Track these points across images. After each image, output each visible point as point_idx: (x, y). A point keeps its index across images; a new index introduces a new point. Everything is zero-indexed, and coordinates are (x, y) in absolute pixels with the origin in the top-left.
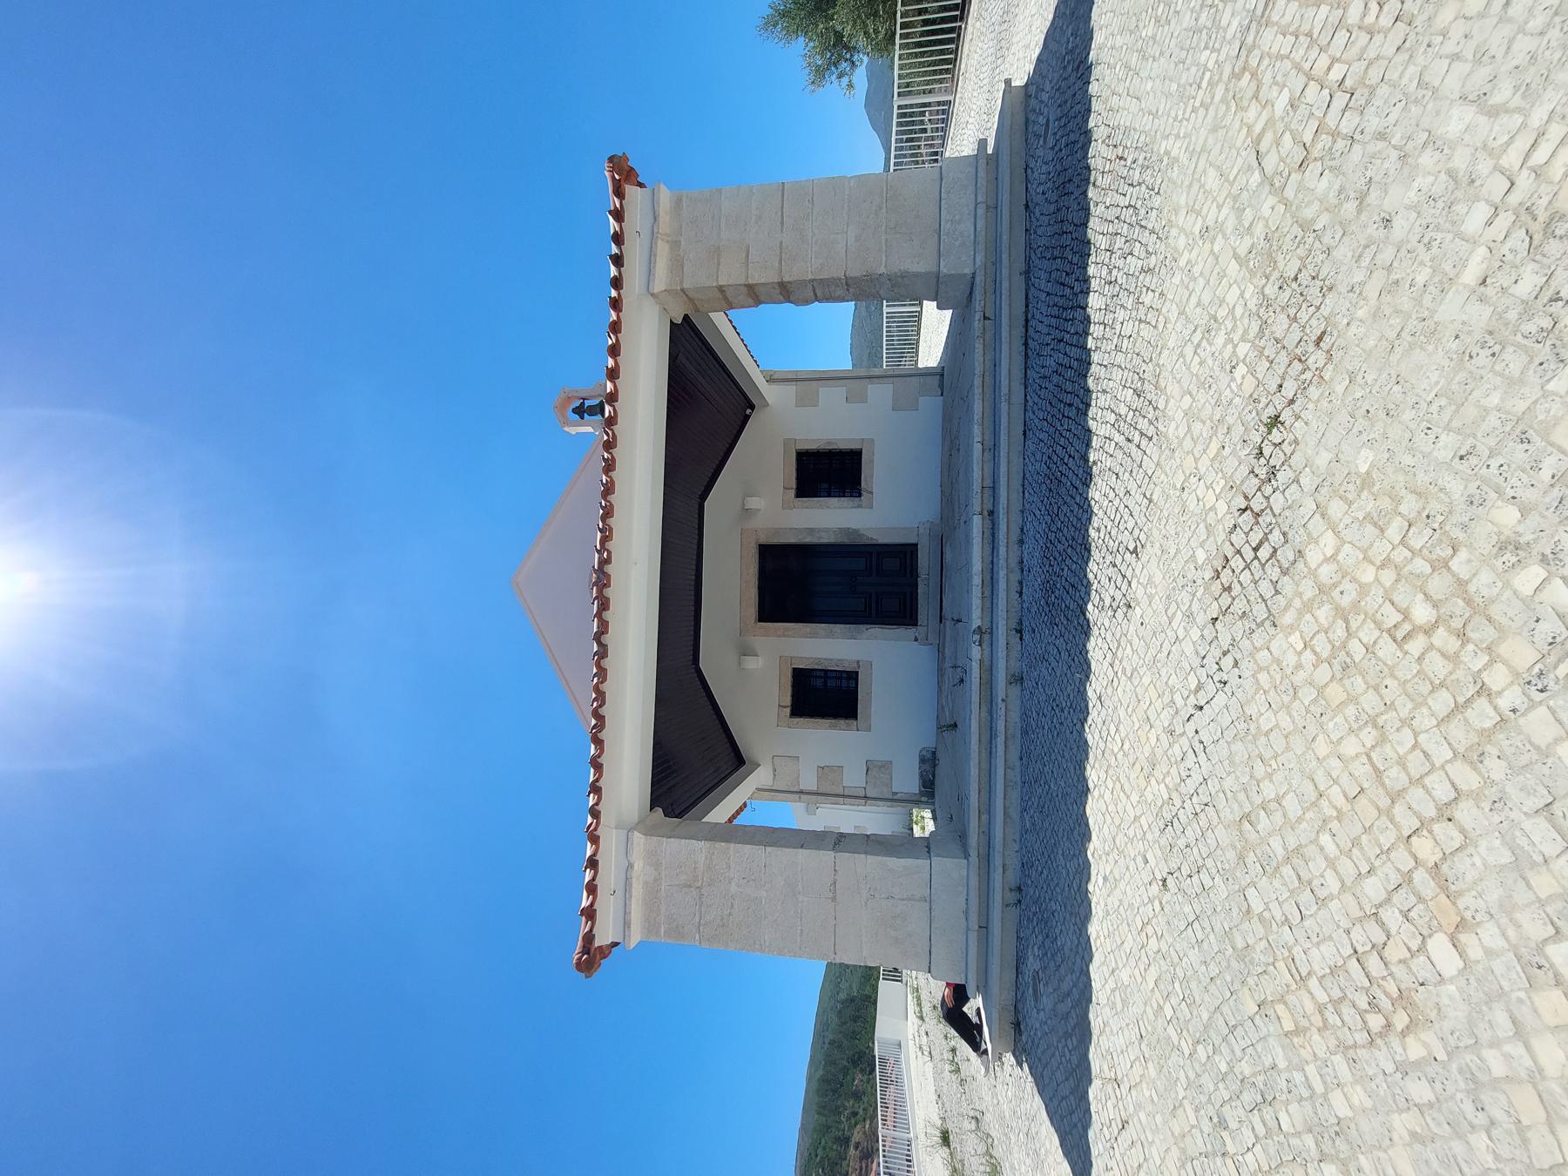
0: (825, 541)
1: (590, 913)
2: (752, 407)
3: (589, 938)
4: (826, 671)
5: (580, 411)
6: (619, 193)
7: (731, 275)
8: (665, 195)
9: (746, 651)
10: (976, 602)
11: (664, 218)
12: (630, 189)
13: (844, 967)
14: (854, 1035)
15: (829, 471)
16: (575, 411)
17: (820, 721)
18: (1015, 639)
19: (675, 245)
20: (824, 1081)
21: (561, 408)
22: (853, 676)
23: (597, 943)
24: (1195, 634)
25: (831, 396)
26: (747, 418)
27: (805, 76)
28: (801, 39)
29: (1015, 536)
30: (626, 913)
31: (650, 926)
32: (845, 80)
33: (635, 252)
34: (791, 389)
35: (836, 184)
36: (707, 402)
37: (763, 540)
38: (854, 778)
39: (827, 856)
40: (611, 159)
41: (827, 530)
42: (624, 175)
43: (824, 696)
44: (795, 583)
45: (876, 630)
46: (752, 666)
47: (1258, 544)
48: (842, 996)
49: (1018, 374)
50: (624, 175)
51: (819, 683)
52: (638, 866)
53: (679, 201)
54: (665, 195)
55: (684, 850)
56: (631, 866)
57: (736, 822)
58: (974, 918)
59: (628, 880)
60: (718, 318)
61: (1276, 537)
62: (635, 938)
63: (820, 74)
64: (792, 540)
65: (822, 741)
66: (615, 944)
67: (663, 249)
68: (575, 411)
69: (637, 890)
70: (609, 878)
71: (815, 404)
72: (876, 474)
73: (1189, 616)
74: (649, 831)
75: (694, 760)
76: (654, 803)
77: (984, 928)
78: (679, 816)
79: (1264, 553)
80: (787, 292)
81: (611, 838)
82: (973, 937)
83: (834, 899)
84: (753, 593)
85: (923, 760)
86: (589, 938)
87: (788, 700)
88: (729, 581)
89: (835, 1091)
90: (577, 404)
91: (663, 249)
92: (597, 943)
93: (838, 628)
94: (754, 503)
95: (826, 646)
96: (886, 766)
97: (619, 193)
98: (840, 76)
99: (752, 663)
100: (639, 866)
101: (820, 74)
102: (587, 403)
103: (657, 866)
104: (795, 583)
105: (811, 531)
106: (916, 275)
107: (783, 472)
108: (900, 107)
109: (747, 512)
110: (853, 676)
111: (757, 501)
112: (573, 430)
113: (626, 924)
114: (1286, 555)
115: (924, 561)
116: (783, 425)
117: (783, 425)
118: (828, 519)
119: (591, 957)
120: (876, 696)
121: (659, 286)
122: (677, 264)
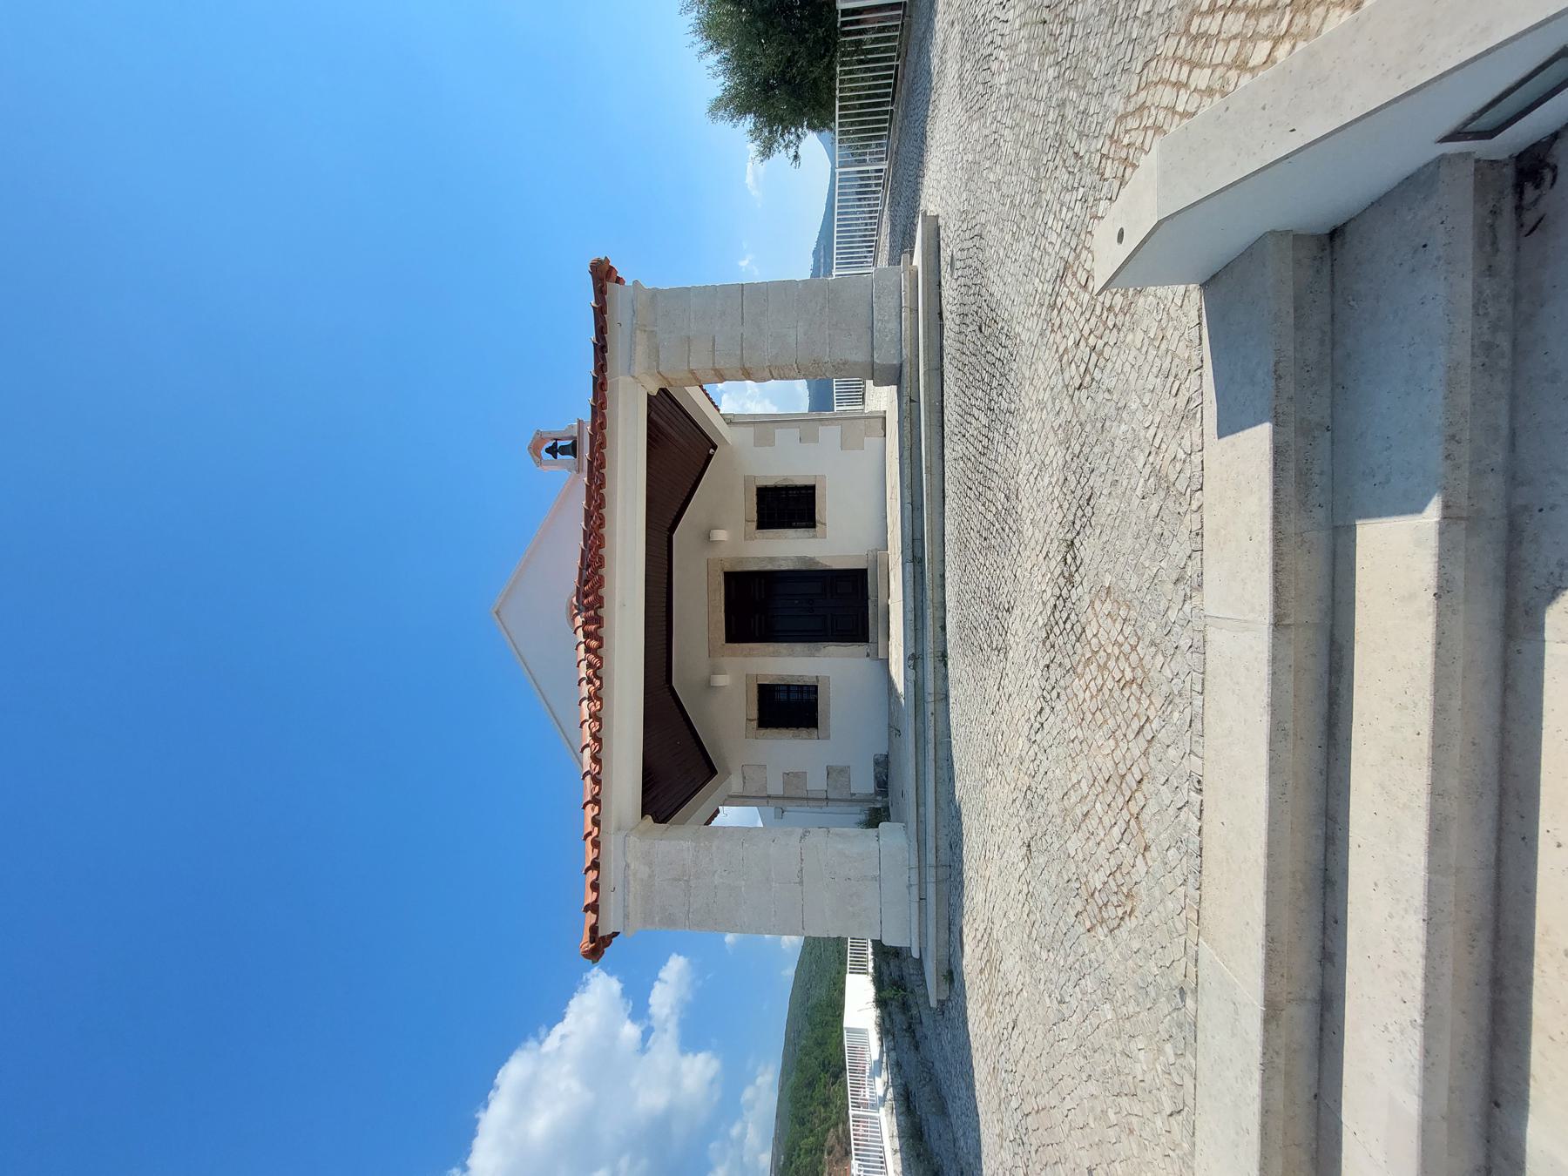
3: (594, 929)
13: (816, 692)
14: (820, 1044)
15: (788, 506)
16: (548, 450)
17: (784, 731)
22: (813, 689)
23: (600, 934)
24: (1039, 673)
26: (710, 457)
27: (753, 148)
34: (749, 431)
37: (728, 568)
41: (786, 559)
43: (788, 708)
48: (813, 1001)
51: (783, 696)
57: (713, 823)
58: (915, 890)
60: (694, 391)
61: (1073, 617)
65: (787, 751)
66: (616, 934)
68: (548, 450)
71: (772, 444)
72: (827, 507)
73: (1036, 661)
75: (678, 770)
76: (645, 811)
78: (664, 821)
79: (1068, 626)
81: (612, 843)
83: (801, 883)
85: (877, 763)
87: (754, 714)
90: (550, 444)
92: (600, 934)
93: (799, 647)
95: (788, 663)
96: (844, 771)
98: (787, 147)
102: (560, 444)
105: (772, 559)
106: (856, 363)
108: (841, 99)
110: (813, 689)
113: (626, 916)
114: (1078, 629)
118: (786, 549)
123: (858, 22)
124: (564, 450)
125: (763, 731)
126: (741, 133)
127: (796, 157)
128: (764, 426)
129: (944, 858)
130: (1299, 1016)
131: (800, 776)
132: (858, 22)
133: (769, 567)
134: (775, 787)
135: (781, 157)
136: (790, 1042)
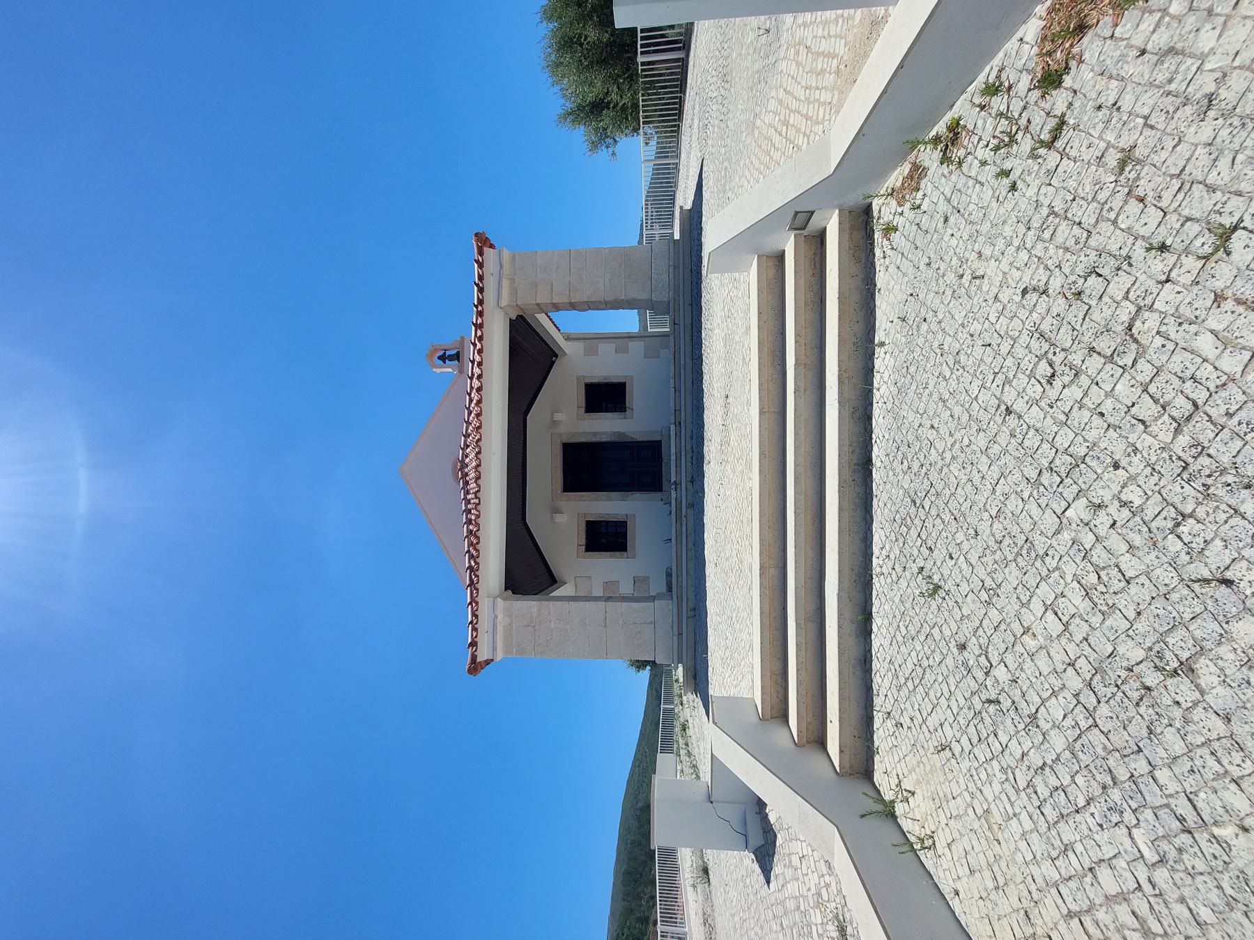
0: (604, 440)
1: (473, 644)
2: (556, 356)
3: (474, 658)
4: (607, 522)
5: (443, 358)
6: (481, 253)
7: (543, 298)
8: (506, 254)
9: (556, 511)
10: (673, 469)
11: (506, 271)
12: (486, 250)
15: (606, 396)
16: (439, 358)
18: (690, 486)
19: (512, 281)
20: (628, 873)
21: (430, 356)
22: (623, 525)
25: (606, 348)
27: (585, 147)
28: (582, 127)
29: (689, 435)
30: (494, 642)
31: (508, 650)
32: (610, 150)
33: (490, 284)
34: (581, 344)
35: (598, 251)
36: (531, 356)
37: (565, 440)
38: (626, 588)
39: (601, 604)
40: (476, 235)
41: (605, 433)
42: (483, 242)
43: (605, 538)
44: (586, 467)
45: (638, 495)
46: (561, 521)
47: (725, 443)
48: (640, 805)
49: (689, 354)
50: (483, 242)
51: (603, 530)
52: (500, 617)
53: (514, 257)
54: (506, 254)
55: (528, 606)
56: (496, 617)
58: (675, 628)
59: (495, 625)
60: (542, 318)
62: (499, 657)
63: (594, 146)
64: (583, 440)
65: (606, 566)
67: (505, 283)
68: (439, 358)
69: (500, 629)
70: (484, 624)
72: (636, 397)
74: (505, 599)
75: (529, 573)
77: (680, 634)
80: (573, 306)
82: (675, 638)
84: (559, 474)
86: (474, 658)
87: (583, 541)
88: (545, 467)
89: (636, 881)
91: (505, 283)
93: (613, 494)
94: (558, 416)
95: (606, 506)
96: (645, 580)
97: (481, 253)
99: (560, 518)
100: (500, 614)
101: (594, 146)
103: (510, 616)
104: (586, 467)
107: (576, 397)
109: (554, 423)
111: (562, 416)
112: (438, 371)
113: (494, 649)
115: (671, 450)
116: (577, 366)
117: (577, 366)
118: (605, 426)
119: (475, 667)
120: (639, 536)
121: (504, 303)
122: (514, 291)
123: (652, 69)
124: (451, 358)
125: (560, 447)
126: (579, 135)
127: (614, 154)
128: (592, 340)
129: (691, 605)
130: (773, 572)
131: (615, 584)
132: (652, 69)
133: (594, 439)
134: (598, 592)
135: (603, 153)
136: (622, 838)
